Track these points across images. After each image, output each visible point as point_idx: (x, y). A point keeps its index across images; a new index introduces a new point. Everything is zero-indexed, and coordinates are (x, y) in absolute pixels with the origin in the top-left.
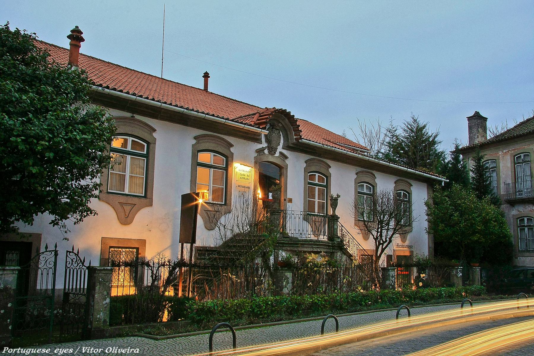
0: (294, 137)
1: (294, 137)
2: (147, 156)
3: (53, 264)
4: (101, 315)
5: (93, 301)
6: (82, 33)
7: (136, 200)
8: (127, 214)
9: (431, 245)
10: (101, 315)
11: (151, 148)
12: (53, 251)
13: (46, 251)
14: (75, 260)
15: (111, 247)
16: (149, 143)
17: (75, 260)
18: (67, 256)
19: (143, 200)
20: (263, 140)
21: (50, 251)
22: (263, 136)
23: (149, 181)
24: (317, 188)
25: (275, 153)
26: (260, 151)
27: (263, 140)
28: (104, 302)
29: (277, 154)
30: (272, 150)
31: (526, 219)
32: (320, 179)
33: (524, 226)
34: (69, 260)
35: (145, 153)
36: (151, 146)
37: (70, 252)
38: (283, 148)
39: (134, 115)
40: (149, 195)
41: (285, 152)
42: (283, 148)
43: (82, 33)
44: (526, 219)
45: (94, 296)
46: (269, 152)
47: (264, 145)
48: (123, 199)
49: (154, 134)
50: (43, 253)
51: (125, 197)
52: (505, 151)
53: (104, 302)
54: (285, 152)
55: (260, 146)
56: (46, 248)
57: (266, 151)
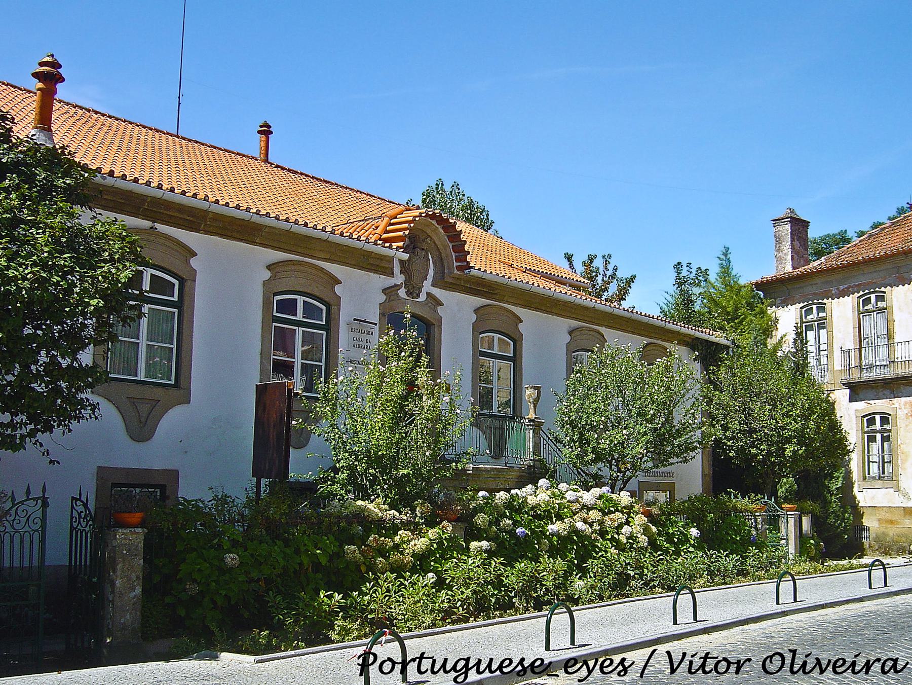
0: (455, 264)
1: (455, 264)
2: (179, 305)
3: (40, 523)
4: (128, 616)
5: (113, 592)
6: (60, 66)
7: (159, 392)
8: (143, 420)
9: (707, 472)
10: (128, 616)
11: (187, 289)
12: (39, 498)
13: (28, 499)
14: (83, 515)
15: (115, 485)
16: (183, 278)
17: (83, 515)
18: (72, 507)
19: (172, 391)
20: (397, 269)
21: (34, 499)
22: (396, 262)
23: (184, 354)
24: (299, 331)
25: (418, 296)
26: (390, 291)
27: (397, 269)
28: (132, 594)
29: (423, 298)
30: (413, 291)
31: (878, 418)
32: (309, 310)
33: (875, 431)
34: (75, 514)
35: (176, 298)
36: (188, 283)
37: (77, 500)
38: (433, 285)
39: (157, 225)
40: (183, 383)
41: (437, 292)
42: (433, 285)
43: (60, 66)
44: (878, 418)
45: (113, 584)
46: (409, 293)
47: (399, 279)
48: (135, 391)
49: (439, 309)
50: (22, 502)
51: (139, 387)
52: (841, 287)
53: (132, 594)
54: (437, 292)
55: (390, 282)
56: (28, 492)
57: (402, 292)
